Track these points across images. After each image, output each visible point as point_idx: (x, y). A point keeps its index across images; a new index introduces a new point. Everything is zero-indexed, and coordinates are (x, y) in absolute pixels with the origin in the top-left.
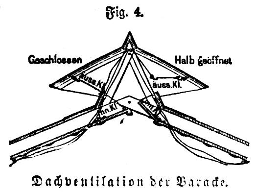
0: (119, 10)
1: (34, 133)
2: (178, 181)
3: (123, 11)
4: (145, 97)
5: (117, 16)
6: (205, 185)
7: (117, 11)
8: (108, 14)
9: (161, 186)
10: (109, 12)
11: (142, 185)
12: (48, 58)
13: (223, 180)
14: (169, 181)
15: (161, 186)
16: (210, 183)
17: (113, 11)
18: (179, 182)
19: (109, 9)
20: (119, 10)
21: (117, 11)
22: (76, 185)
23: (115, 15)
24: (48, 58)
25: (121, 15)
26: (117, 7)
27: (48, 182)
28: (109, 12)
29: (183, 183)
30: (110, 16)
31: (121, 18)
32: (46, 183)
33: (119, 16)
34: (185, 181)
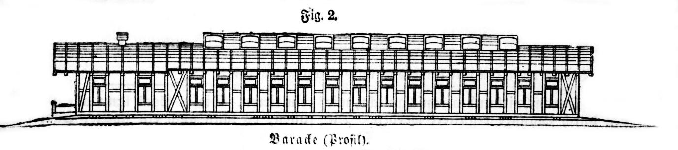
0: (314, 12)
1: (539, 125)
2: (272, 138)
3: (318, 14)
4: (151, 69)
5: (312, 19)
6: (284, 143)
7: (312, 14)
8: (303, 17)
9: (315, 143)
10: (304, 15)
11: (287, 143)
12: (335, 16)
13: (315, 138)
14: (294, 138)
15: (315, 143)
16: (303, 141)
17: (308, 14)
18: (273, 140)
19: (304, 12)
20: (314, 12)
21: (312, 14)
22: (292, 143)
23: (310, 18)
24: (335, 16)
25: (316, 18)
26: (312, 10)
27: (285, 139)
28: (304, 15)
29: (276, 141)
30: (305, 19)
31: (316, 21)
32: (306, 141)
33: (314, 19)
34: (278, 138)
